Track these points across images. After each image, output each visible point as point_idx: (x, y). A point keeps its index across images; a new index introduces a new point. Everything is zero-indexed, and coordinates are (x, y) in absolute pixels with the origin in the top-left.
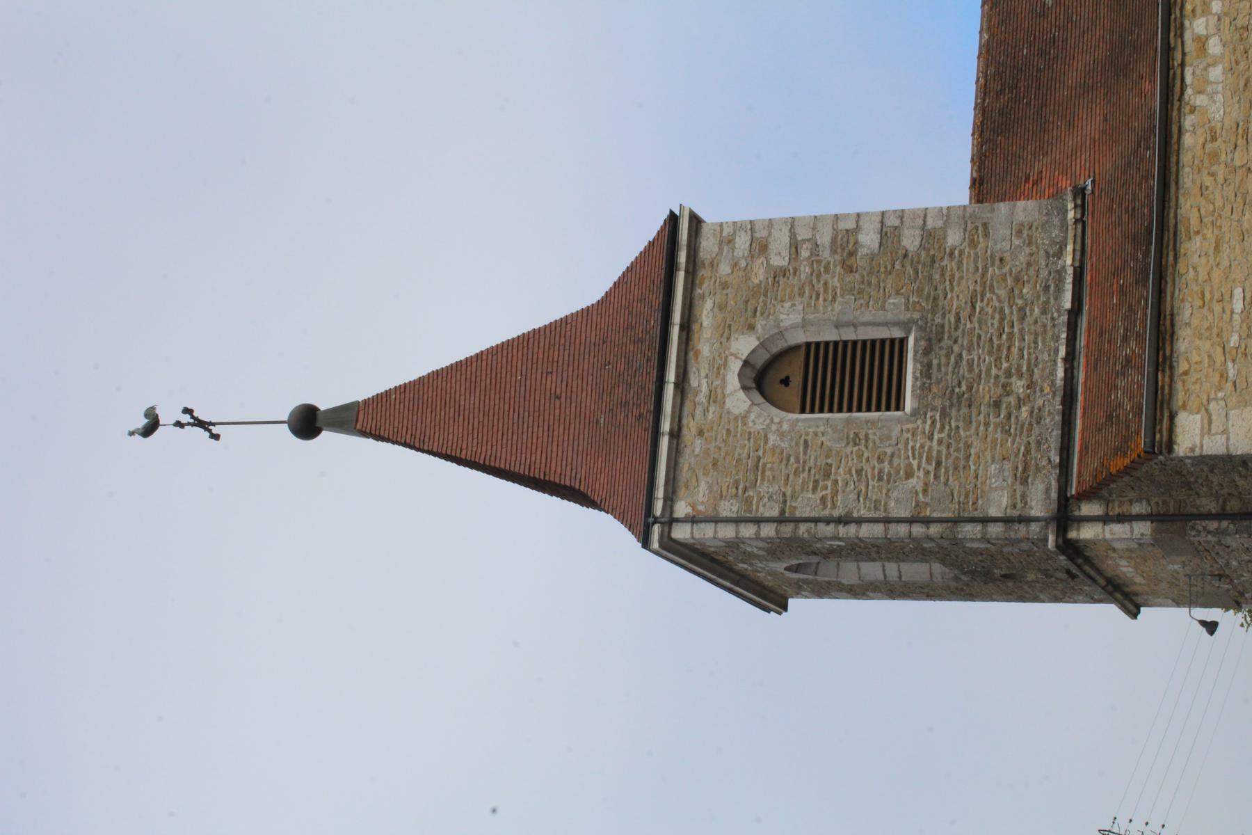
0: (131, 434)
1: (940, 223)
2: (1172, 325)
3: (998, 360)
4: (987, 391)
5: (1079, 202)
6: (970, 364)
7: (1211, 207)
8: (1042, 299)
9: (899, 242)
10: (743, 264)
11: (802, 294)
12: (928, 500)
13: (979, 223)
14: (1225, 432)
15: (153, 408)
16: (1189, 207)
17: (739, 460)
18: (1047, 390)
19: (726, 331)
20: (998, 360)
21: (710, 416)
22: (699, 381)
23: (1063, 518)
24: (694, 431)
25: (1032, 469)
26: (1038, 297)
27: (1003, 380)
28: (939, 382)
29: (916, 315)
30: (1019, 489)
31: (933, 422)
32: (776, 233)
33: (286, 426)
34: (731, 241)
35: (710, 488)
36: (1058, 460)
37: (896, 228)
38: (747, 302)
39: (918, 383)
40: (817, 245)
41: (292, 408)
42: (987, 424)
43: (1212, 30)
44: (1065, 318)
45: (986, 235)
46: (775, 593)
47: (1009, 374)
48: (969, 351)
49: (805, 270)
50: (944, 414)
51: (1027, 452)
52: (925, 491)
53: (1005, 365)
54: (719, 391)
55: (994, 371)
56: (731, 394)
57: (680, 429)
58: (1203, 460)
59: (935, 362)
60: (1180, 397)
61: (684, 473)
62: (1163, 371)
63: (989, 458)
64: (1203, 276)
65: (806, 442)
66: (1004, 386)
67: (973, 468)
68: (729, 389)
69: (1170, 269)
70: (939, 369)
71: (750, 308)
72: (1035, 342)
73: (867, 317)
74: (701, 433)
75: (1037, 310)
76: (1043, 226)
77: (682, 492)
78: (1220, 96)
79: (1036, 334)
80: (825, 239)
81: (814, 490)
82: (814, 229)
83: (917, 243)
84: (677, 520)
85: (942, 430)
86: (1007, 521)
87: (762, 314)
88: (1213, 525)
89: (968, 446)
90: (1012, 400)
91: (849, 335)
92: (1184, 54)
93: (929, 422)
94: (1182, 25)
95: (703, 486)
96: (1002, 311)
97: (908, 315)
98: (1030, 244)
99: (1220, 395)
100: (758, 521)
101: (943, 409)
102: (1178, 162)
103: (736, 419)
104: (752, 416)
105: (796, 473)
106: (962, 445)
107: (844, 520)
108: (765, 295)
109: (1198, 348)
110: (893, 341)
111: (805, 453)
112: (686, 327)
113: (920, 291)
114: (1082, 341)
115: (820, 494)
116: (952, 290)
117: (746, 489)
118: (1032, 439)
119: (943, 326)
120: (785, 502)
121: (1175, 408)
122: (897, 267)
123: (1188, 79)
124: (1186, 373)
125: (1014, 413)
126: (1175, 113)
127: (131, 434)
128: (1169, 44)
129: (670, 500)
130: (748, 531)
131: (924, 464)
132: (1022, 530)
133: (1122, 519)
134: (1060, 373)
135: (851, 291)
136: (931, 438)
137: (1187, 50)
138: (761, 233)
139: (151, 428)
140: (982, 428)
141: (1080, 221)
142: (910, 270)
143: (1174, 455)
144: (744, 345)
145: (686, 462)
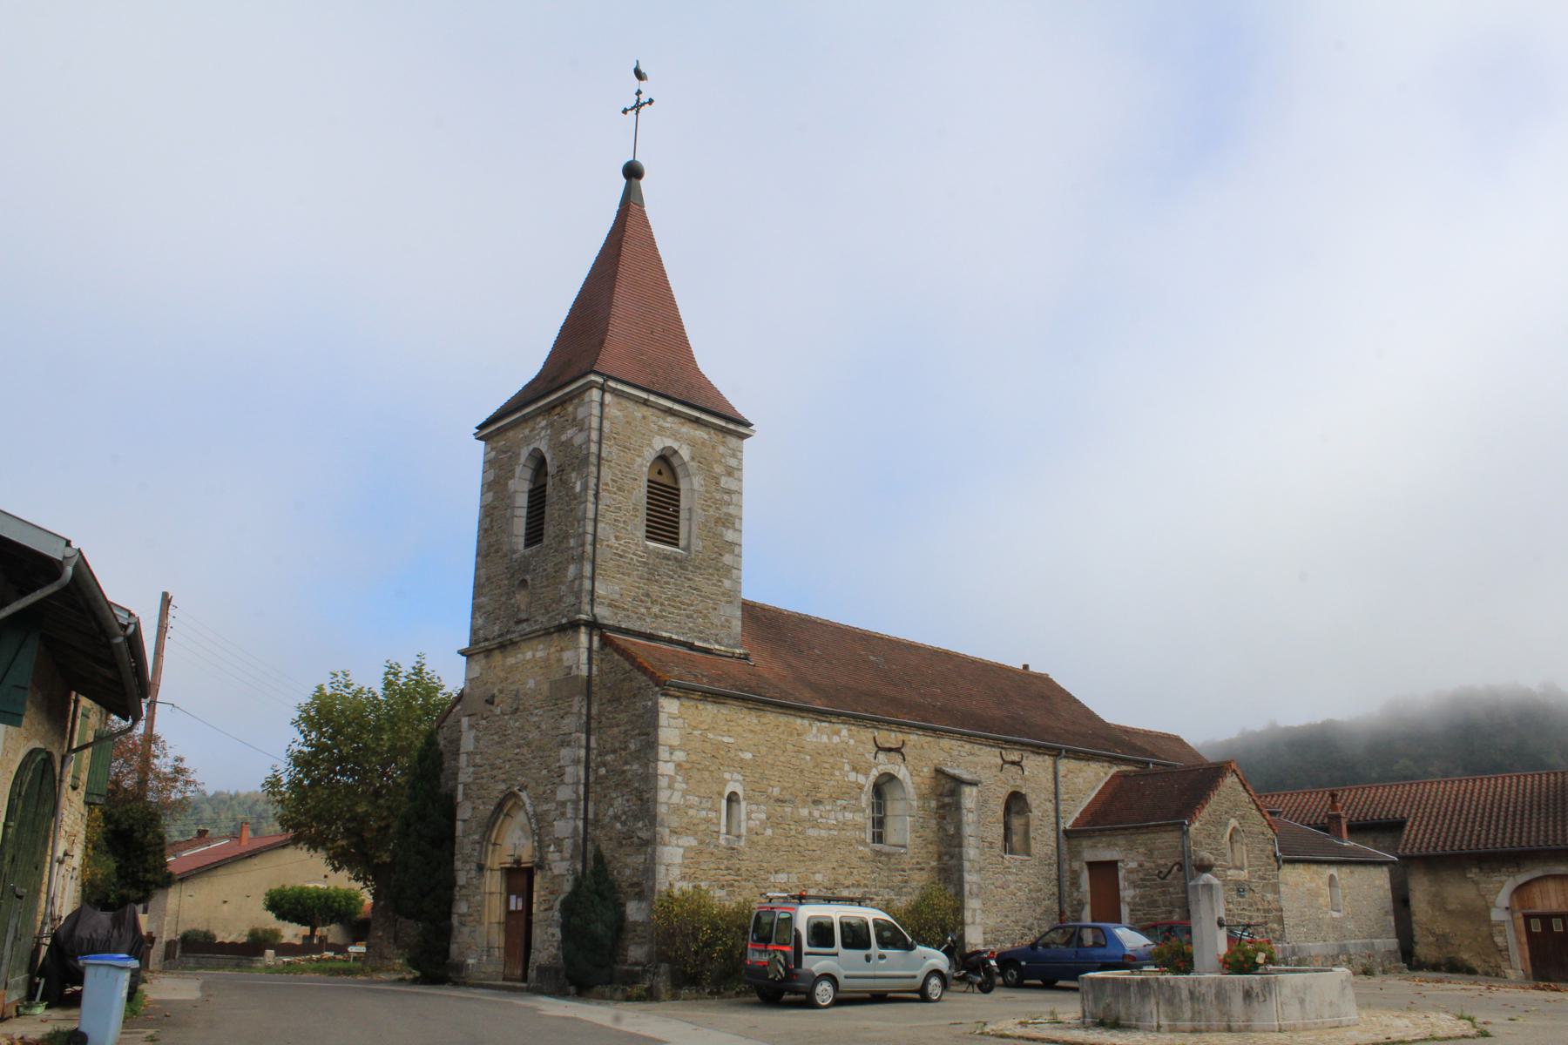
0: (638, 62)
1: (734, 577)
2: (719, 703)
3: (669, 599)
4: (655, 589)
5: (742, 656)
6: (667, 583)
7: (770, 730)
8: (696, 629)
9: (727, 552)
10: (723, 461)
11: (707, 492)
12: (604, 547)
13: (732, 599)
14: (669, 726)
15: (647, 79)
16: (771, 718)
17: (629, 437)
18: (654, 625)
19: (692, 443)
20: (669, 599)
21: (652, 425)
22: (670, 422)
23: (593, 625)
24: (645, 414)
25: (615, 611)
26: (698, 627)
27: (659, 600)
28: (661, 563)
29: (693, 556)
30: (606, 602)
31: (641, 557)
32: (736, 482)
33: (632, 159)
34: (734, 456)
35: (616, 417)
36: (623, 626)
37: (733, 551)
38: (705, 459)
39: (661, 551)
40: (729, 505)
41: (643, 164)
42: (639, 588)
43: (843, 739)
44: (690, 641)
45: (727, 602)
46: (496, 435)
47: (662, 604)
48: (674, 584)
49: (718, 496)
50: (645, 563)
51: (624, 609)
52: (608, 546)
53: (666, 603)
54: (664, 433)
55: (664, 596)
56: (662, 440)
57: (648, 406)
58: (654, 713)
59: (670, 563)
60: (687, 703)
61: (625, 403)
62: (700, 696)
63: (622, 586)
64: (741, 722)
65: (636, 480)
66: (656, 601)
67: (618, 576)
68: (665, 439)
69: (745, 705)
70: (667, 565)
71: (702, 460)
72: (676, 622)
73: (694, 528)
74: (644, 417)
75: (691, 625)
76: (729, 635)
77: (616, 399)
78: (815, 740)
79: (679, 623)
80: (732, 510)
81: (612, 480)
82: (736, 505)
83: (727, 563)
84: (603, 394)
85: (639, 562)
86: (592, 592)
87: (699, 466)
88: (584, 711)
89: (629, 575)
90: (649, 604)
91: (683, 515)
92: (834, 723)
93: (642, 554)
94: (846, 723)
95: (619, 413)
96: (692, 605)
97: (693, 552)
98: (722, 626)
99: (686, 725)
100: (600, 443)
101: (647, 564)
102: (791, 715)
103: (650, 440)
104: (651, 450)
105: (621, 471)
106: (630, 571)
107: (596, 495)
108: (708, 471)
109: (708, 715)
110: (677, 539)
111: (631, 478)
112: (697, 421)
113: (704, 560)
114: (679, 649)
115: (610, 483)
116: (703, 578)
117: (615, 438)
118: (629, 613)
119: (687, 570)
120: (607, 461)
121: (682, 700)
122: (716, 549)
123: (823, 724)
124: (697, 707)
125: (643, 605)
126: (811, 715)
127: (638, 62)
128: (841, 716)
129: (614, 392)
130: (594, 436)
131: (622, 547)
132: (586, 599)
133: (590, 659)
134: (664, 634)
135: (707, 521)
136: (634, 554)
137: (836, 725)
138: (736, 474)
139: (639, 75)
140: (637, 585)
141: (733, 656)
142: (714, 556)
143: (659, 696)
144: (685, 453)
145: (630, 405)
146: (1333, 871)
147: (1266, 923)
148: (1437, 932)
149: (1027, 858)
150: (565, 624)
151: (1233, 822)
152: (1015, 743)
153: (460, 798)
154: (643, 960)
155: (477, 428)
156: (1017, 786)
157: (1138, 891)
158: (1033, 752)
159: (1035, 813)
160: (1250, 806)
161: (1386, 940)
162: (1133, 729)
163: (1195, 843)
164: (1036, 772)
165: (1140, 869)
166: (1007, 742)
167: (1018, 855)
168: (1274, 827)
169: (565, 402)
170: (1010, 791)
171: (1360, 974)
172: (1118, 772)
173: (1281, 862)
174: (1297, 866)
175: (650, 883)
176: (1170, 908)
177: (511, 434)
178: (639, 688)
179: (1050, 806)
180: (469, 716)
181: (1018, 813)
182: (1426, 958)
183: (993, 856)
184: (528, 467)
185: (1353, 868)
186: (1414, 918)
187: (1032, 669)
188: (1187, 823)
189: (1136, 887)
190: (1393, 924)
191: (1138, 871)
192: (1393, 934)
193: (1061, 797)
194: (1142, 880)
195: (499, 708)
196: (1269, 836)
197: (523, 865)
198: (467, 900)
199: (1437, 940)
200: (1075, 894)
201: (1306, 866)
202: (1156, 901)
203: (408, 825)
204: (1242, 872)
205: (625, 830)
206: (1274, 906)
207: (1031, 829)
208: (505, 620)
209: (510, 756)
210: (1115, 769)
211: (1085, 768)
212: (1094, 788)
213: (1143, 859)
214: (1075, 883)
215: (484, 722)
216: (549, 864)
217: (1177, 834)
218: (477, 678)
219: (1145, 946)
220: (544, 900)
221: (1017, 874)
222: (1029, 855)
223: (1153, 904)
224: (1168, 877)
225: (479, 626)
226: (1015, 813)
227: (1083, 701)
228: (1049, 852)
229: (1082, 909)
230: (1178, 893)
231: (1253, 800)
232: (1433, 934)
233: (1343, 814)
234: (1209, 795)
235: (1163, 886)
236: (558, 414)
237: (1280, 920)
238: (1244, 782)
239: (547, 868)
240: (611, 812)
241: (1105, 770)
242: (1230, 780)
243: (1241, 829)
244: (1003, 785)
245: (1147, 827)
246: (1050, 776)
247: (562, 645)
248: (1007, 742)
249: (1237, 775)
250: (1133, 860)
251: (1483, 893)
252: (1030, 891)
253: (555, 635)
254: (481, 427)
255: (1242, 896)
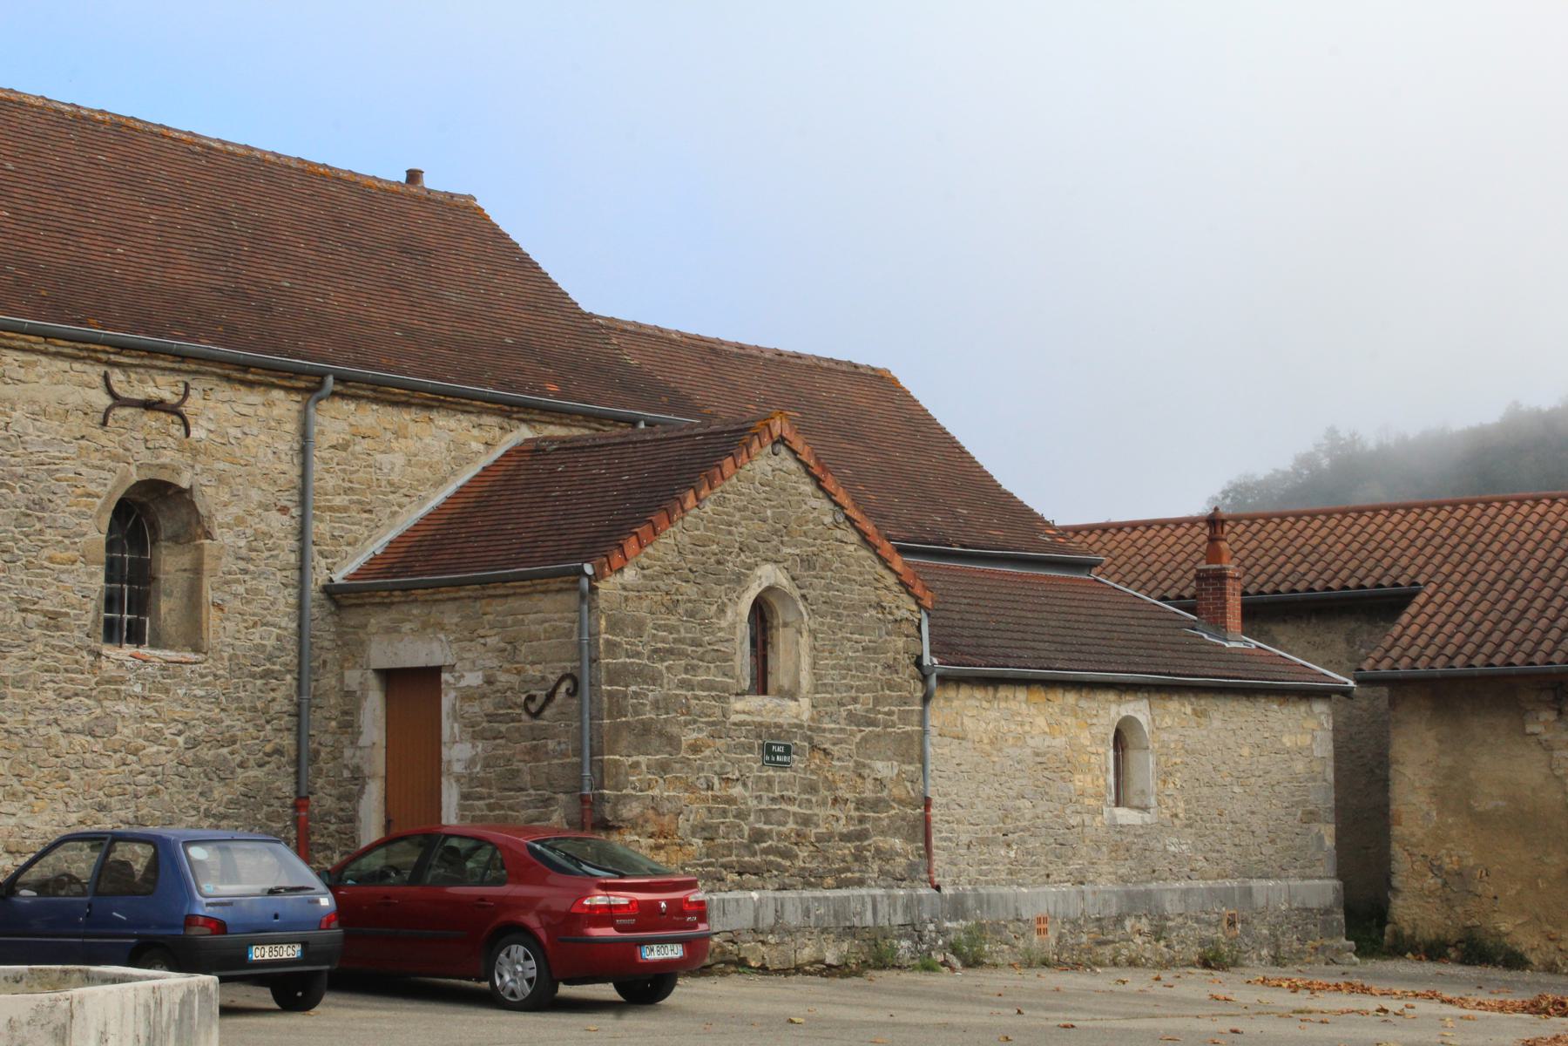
146: (1137, 709)
147: (862, 835)
148: (1447, 867)
149: (192, 657)
151: (768, 575)
152: (152, 352)
156: (163, 467)
157: (480, 745)
158: (228, 379)
159: (225, 539)
160: (838, 533)
161: (1299, 882)
162: (741, 347)
163: (614, 626)
164: (233, 432)
165: (486, 688)
166: (122, 348)
167: (172, 648)
168: (918, 591)
170: (135, 478)
171: (1193, 965)
172: (527, 441)
173: (933, 681)
174: (1003, 692)
176: (547, 794)
179: (280, 525)
181: (175, 539)
182: (1415, 928)
183: (62, 650)
185: (1204, 702)
186: (1396, 831)
187: (430, 182)
188: (588, 569)
189: (477, 736)
190: (1329, 842)
191: (484, 696)
192: (1327, 865)
193: (314, 499)
194: (491, 717)
196: (899, 614)
199: (1445, 884)
200: (348, 753)
201: (1039, 695)
202: (516, 773)
204: (792, 704)
206: (896, 792)
207: (207, 583)
210: (523, 433)
211: (413, 428)
212: (443, 481)
213: (496, 663)
214: (349, 725)
217: (571, 599)
219: (272, 892)
221: (145, 698)
222: (197, 649)
223: (510, 780)
224: (547, 713)
226: (168, 539)
227: (546, 267)
228: (270, 643)
229: (361, 791)
230: (564, 754)
231: (847, 518)
232: (1435, 868)
233: (1231, 568)
234: (682, 502)
235: (535, 734)
237: (923, 830)
238: (817, 471)
241: (487, 436)
242: (764, 464)
243: (796, 593)
244: (110, 464)
245: (505, 580)
246: (287, 443)
248: (122, 348)
249: (794, 452)
250: (474, 667)
251: (1560, 772)
252: (193, 743)
255: (784, 766)
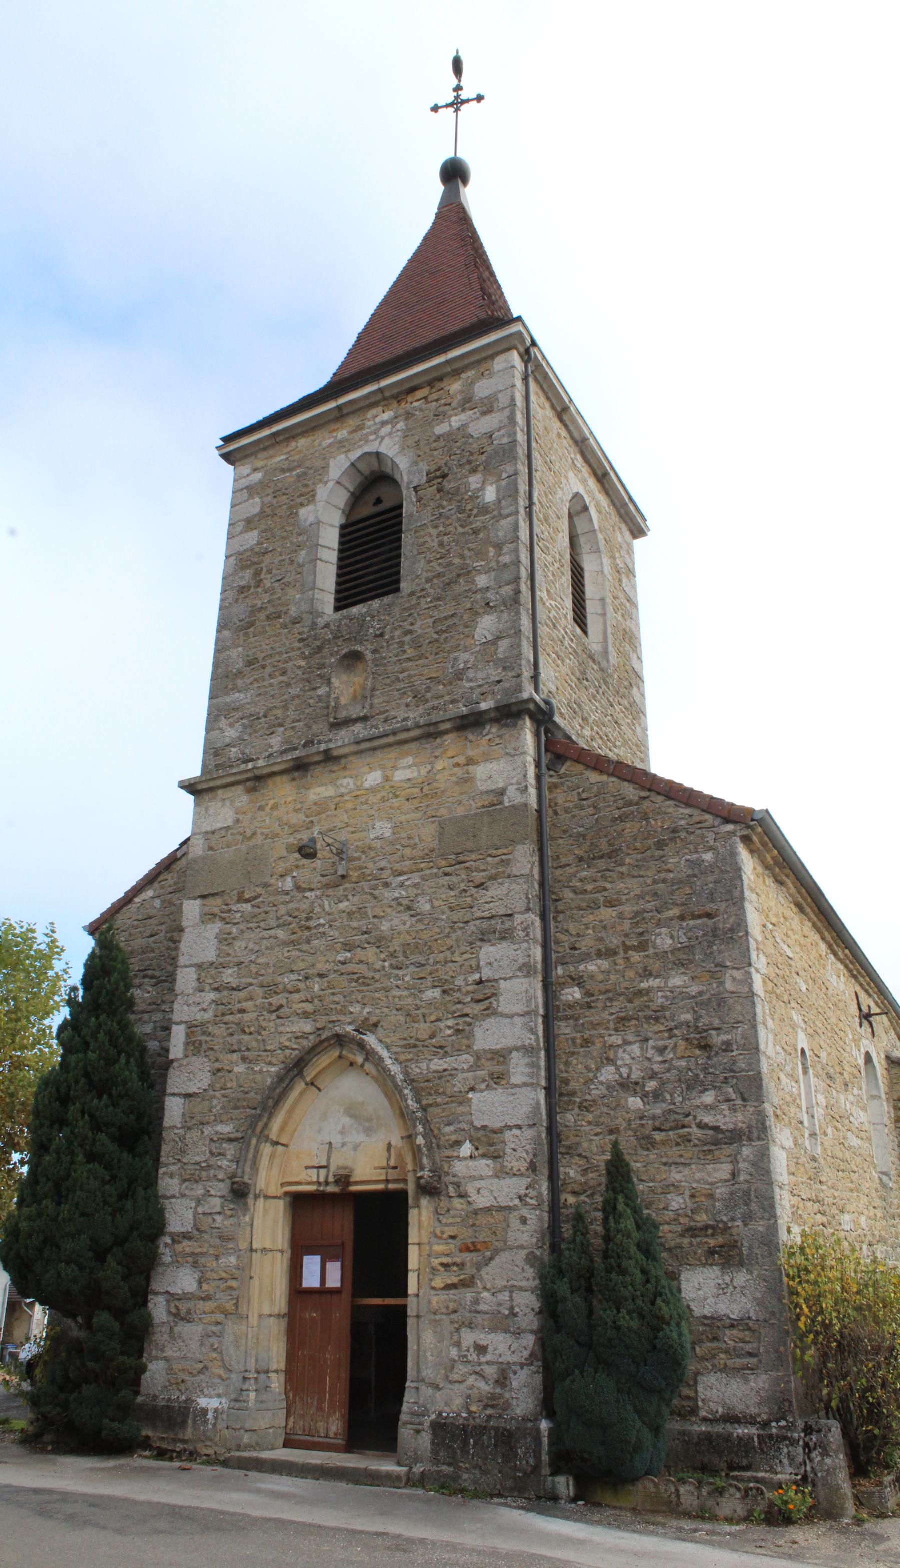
150: (485, 712)
153: (177, 1048)
154: (754, 1410)
155: (223, 439)
169: (440, 379)
175: (760, 1227)
177: (302, 442)
178: (675, 831)
180: (204, 897)
184: (346, 488)
195: (289, 879)
197: (354, 1188)
198: (195, 1265)
203: (65, 1100)
205: (658, 1109)
208: (300, 725)
209: (322, 966)
215: (247, 907)
216: (458, 1185)
218: (228, 828)
220: (445, 1265)
225: (228, 741)
236: (425, 398)
239: (452, 1191)
240: (608, 1074)
247: (470, 753)
253: (449, 739)
254: (228, 439)
